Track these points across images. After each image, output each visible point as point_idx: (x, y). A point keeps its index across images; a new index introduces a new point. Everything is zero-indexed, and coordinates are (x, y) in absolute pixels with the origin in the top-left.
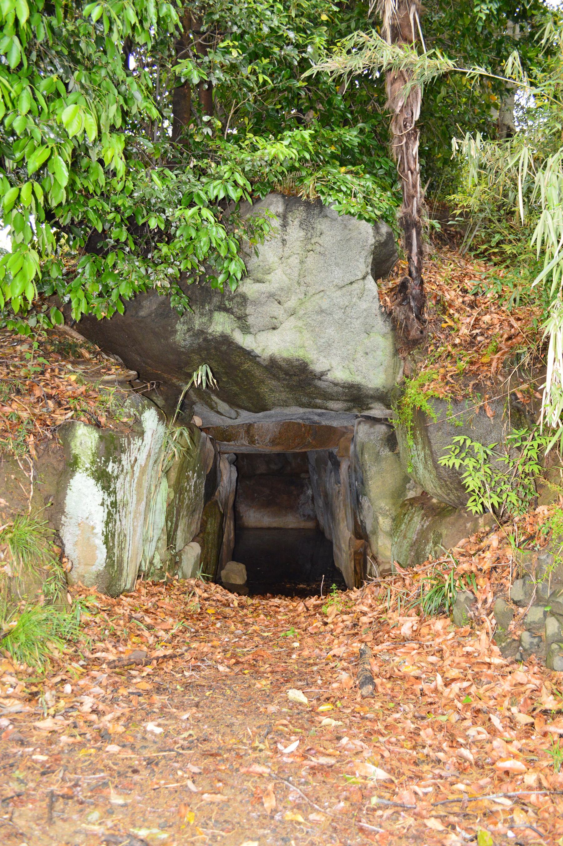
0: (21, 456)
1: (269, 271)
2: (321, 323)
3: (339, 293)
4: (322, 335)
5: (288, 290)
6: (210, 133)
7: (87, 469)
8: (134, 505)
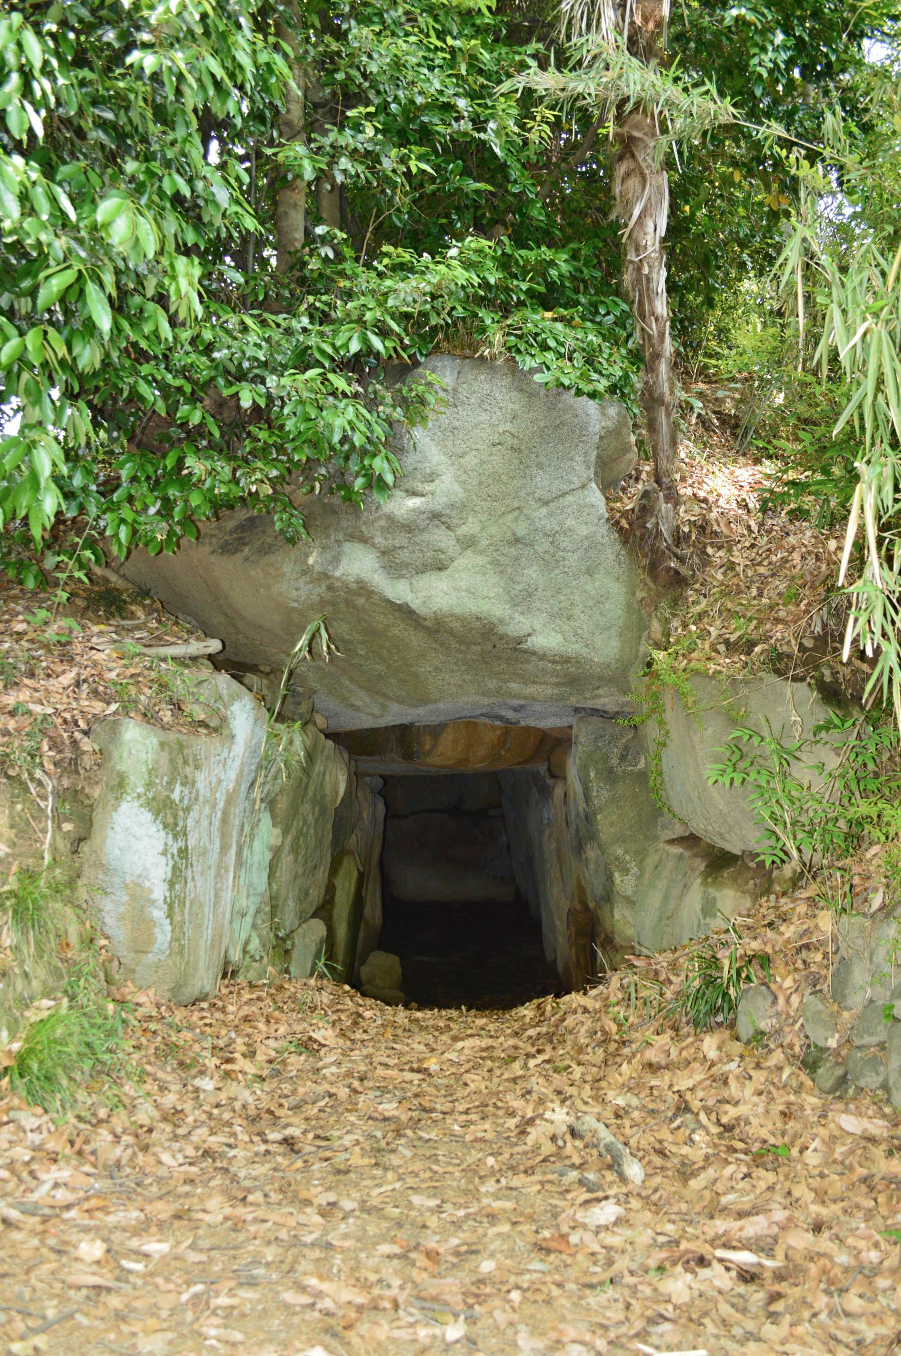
0: (31, 774)
1: (431, 478)
2: (516, 559)
3: (544, 511)
4: (518, 579)
5: (462, 508)
6: (331, 255)
7: (139, 796)
8: (216, 856)
